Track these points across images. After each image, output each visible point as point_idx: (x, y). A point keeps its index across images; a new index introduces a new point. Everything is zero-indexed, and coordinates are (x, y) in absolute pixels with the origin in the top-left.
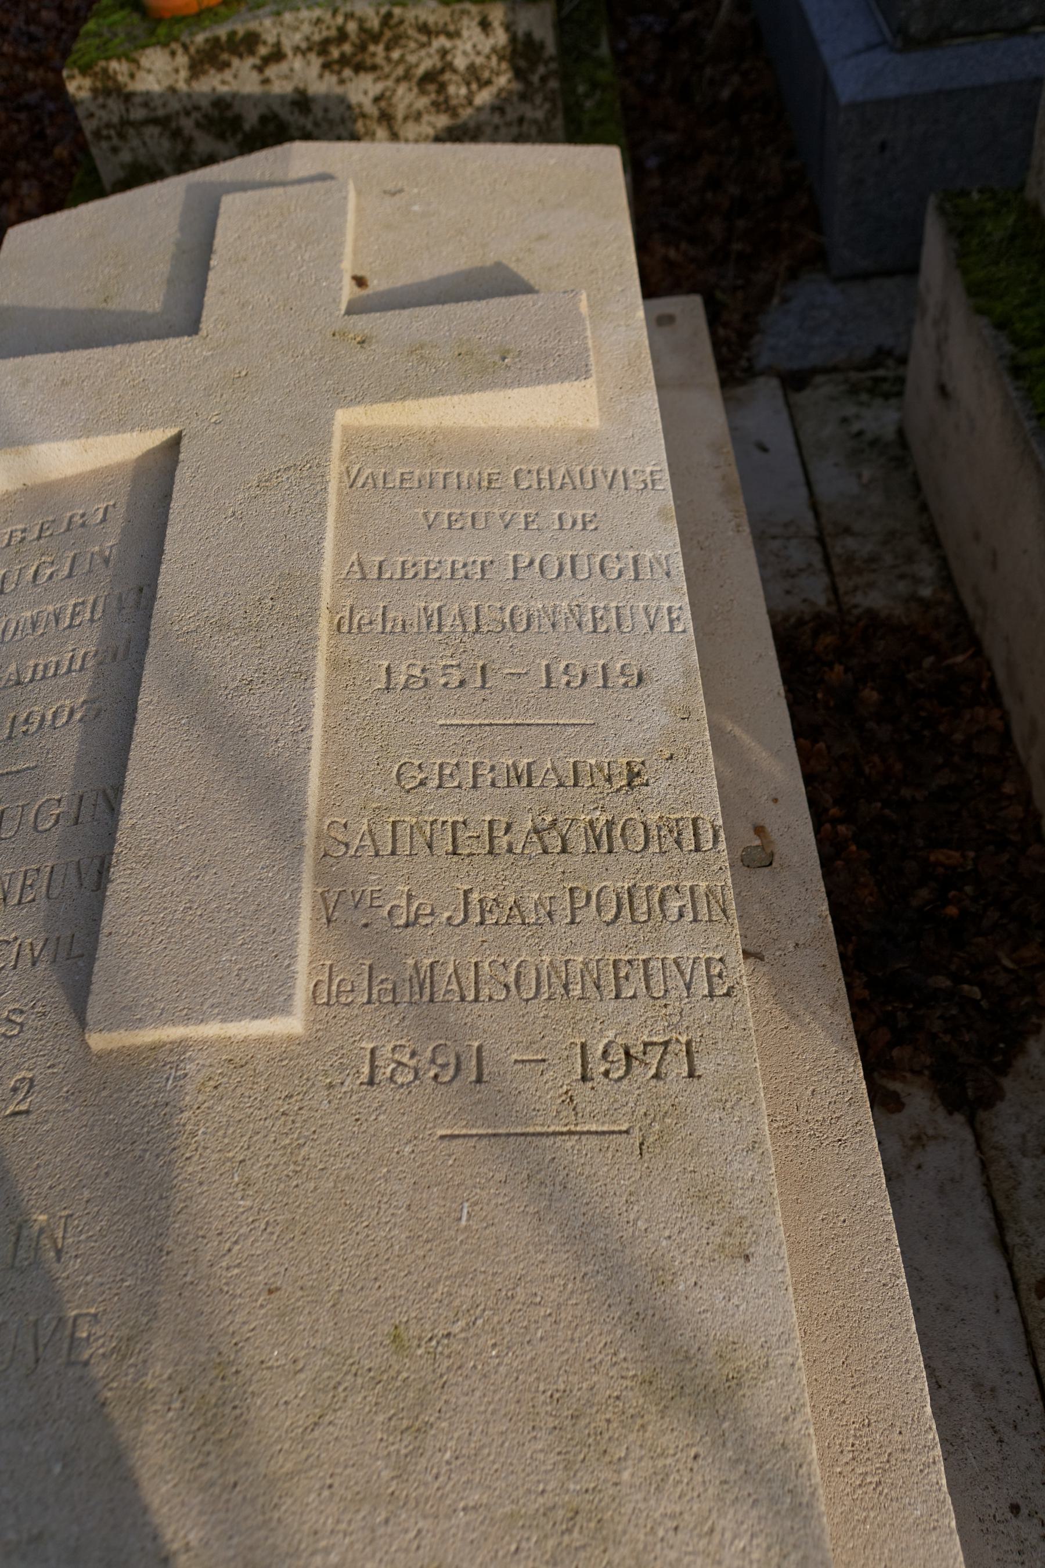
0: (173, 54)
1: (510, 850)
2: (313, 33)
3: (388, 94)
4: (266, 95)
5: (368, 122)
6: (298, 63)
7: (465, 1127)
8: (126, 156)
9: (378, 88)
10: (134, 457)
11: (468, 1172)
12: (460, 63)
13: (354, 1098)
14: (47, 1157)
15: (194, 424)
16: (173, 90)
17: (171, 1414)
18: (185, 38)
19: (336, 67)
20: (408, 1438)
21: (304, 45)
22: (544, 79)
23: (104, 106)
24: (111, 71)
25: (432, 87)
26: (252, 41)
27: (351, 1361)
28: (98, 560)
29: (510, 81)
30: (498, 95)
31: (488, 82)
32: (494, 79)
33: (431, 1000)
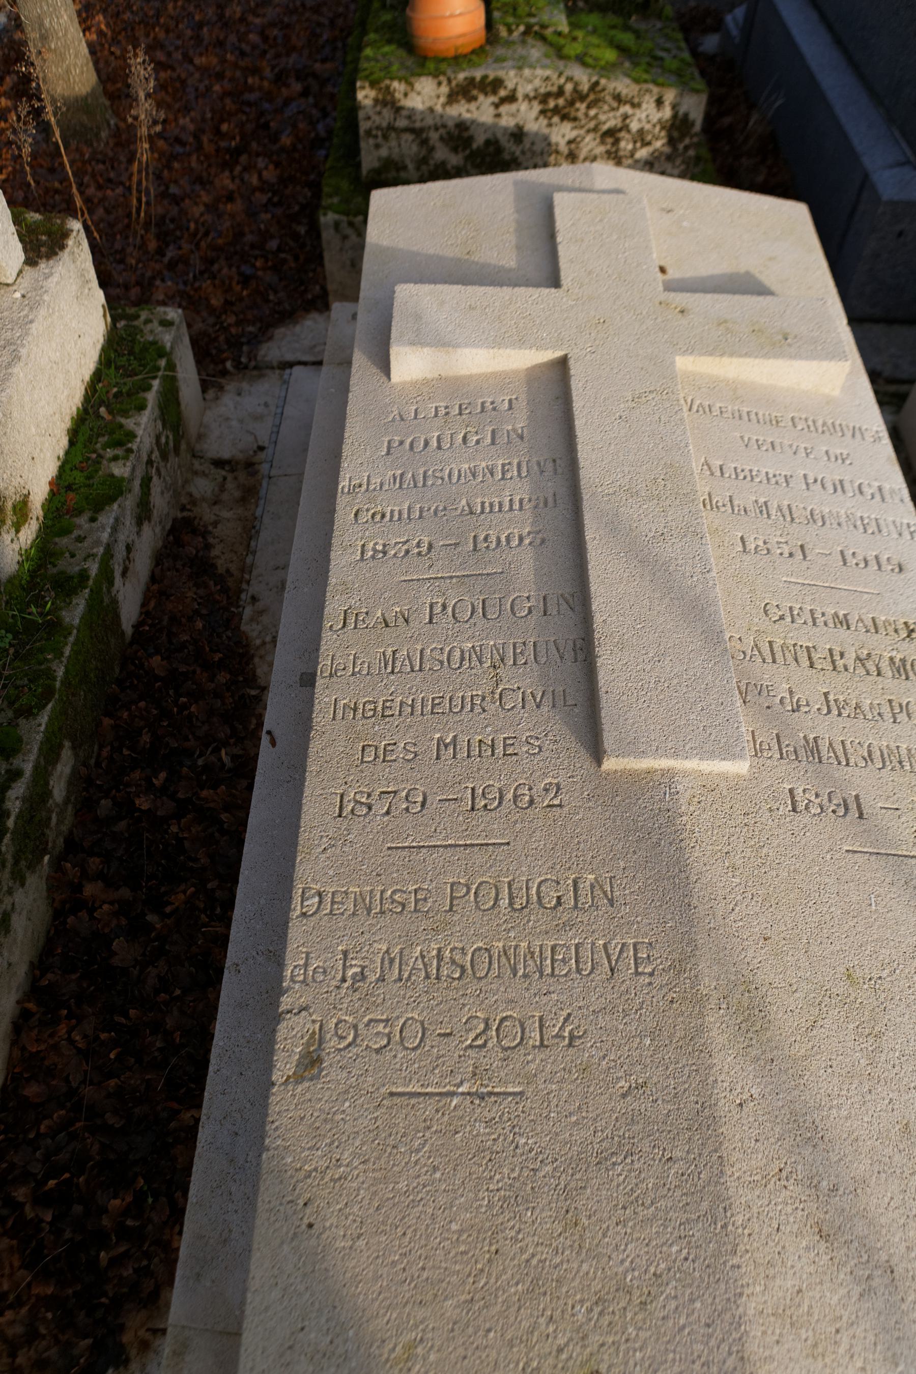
0: (439, 84)
1: (846, 670)
2: (540, 87)
3: (579, 139)
4: (495, 125)
5: (559, 157)
6: (524, 106)
7: (860, 846)
8: (384, 152)
9: (573, 134)
10: (525, 367)
11: (868, 875)
12: (634, 126)
13: (788, 819)
14: (584, 837)
15: (575, 351)
16: (431, 110)
17: (722, 1011)
18: (449, 72)
19: (549, 114)
20: (871, 1040)
21: (532, 94)
22: (686, 148)
23: (379, 113)
24: (392, 88)
25: (610, 140)
26: (497, 84)
27: (825, 988)
28: (513, 436)
29: (663, 145)
30: (653, 153)
31: (649, 144)
32: (653, 142)
33: (820, 762)
